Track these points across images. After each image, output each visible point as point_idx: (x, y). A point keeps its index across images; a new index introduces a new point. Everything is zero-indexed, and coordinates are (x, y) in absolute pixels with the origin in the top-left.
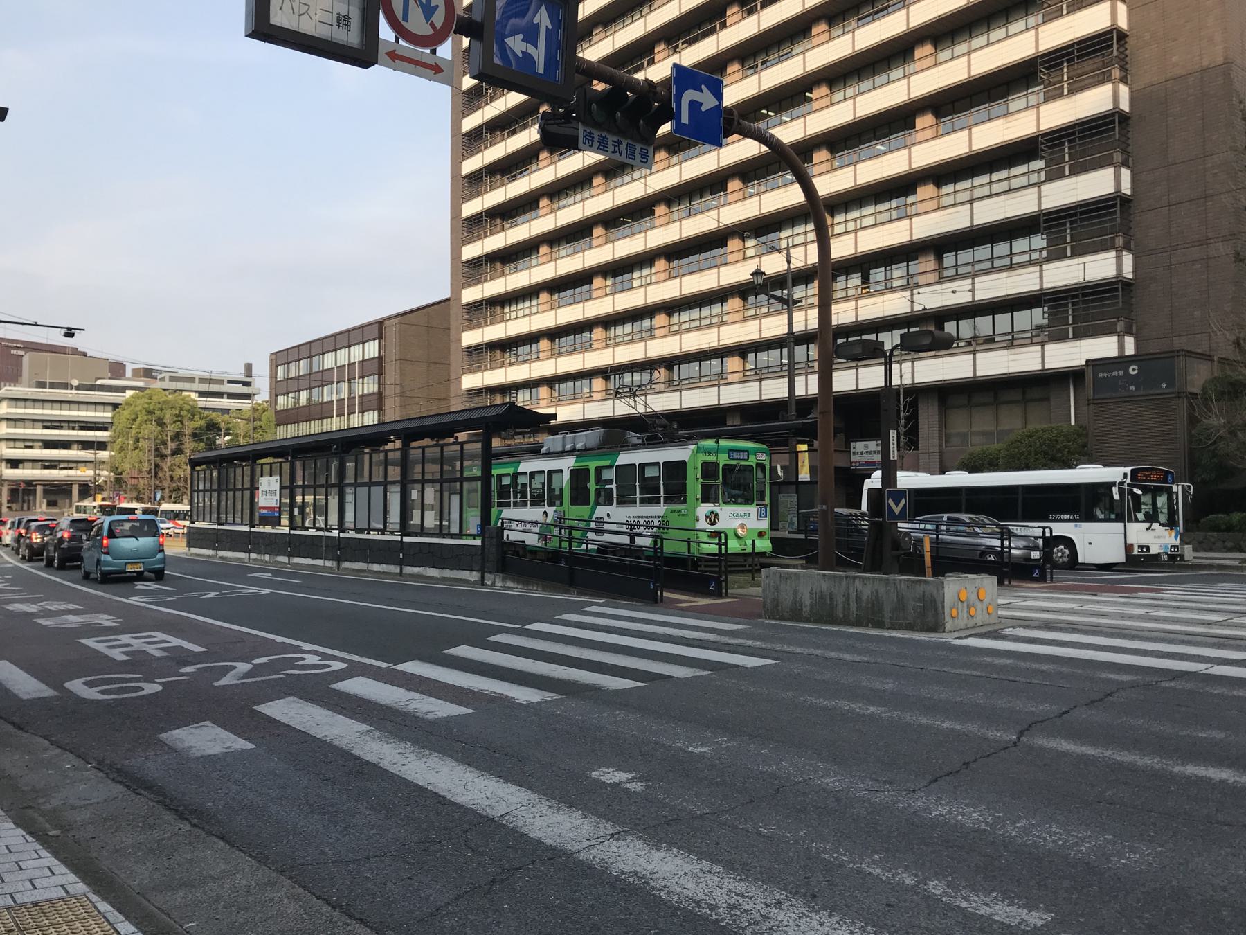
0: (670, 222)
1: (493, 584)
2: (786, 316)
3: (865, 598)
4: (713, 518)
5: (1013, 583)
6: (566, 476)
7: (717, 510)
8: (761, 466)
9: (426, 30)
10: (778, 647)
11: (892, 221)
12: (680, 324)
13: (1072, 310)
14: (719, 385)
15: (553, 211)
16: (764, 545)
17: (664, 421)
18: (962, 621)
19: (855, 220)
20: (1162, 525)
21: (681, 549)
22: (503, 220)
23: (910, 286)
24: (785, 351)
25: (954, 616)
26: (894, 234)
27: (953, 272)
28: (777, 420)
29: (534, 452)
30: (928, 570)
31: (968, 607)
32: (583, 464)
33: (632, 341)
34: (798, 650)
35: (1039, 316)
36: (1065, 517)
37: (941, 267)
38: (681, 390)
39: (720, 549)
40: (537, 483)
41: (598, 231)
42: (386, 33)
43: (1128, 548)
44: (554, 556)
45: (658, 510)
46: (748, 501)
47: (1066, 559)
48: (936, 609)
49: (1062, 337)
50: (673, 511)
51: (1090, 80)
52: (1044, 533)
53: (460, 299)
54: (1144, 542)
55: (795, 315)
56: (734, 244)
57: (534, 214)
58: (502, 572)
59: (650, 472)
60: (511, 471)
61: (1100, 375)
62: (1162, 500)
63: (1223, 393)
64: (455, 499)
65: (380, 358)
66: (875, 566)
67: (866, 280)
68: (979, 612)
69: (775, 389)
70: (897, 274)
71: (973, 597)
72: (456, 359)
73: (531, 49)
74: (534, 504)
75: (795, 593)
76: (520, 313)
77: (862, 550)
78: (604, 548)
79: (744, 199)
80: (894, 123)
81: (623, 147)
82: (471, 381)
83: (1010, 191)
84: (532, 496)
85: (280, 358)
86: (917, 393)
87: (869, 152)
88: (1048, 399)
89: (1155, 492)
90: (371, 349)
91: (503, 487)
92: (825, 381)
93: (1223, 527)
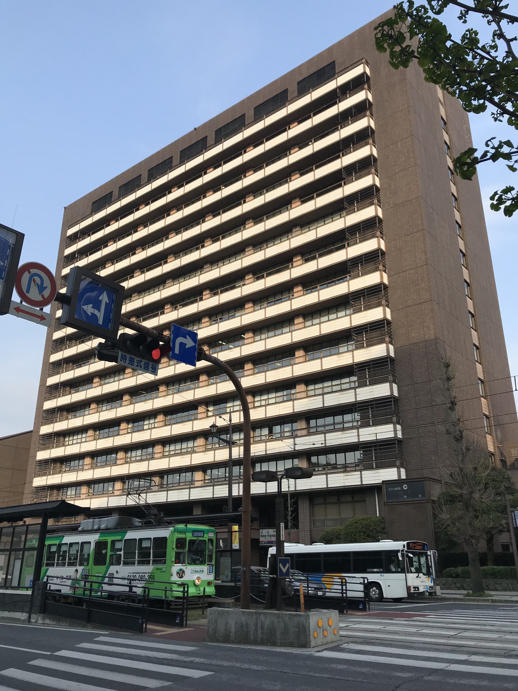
0: (167, 395)
1: (36, 622)
2: (228, 449)
3: (266, 626)
4: (181, 573)
5: (349, 612)
6: (93, 546)
7: (184, 568)
8: (211, 540)
9: (39, 298)
10: (214, 662)
11: (284, 401)
12: (169, 451)
13: (375, 453)
14: (190, 488)
15: (101, 385)
16: (210, 590)
17: (155, 511)
18: (320, 641)
19: (265, 400)
20: (424, 574)
21: (161, 595)
22: (71, 388)
23: (294, 436)
24: (227, 469)
25: (316, 637)
26: (285, 409)
27: (315, 430)
28: (222, 512)
29: (74, 530)
30: (302, 606)
31: (323, 631)
32: (103, 538)
33: (141, 460)
34: (226, 664)
35: (358, 454)
36: (375, 570)
37: (308, 427)
38: (167, 491)
39: (184, 594)
40: (73, 551)
41: (126, 397)
42: (16, 297)
43: (408, 588)
44: (79, 601)
45: (148, 569)
46: (202, 563)
47: (377, 596)
48: (306, 633)
49: (369, 468)
50: (158, 569)
51: (376, 341)
52: (364, 581)
53: (39, 432)
54: (416, 585)
55: (233, 449)
56: (201, 409)
57: (89, 386)
58: (43, 613)
59: (145, 544)
60: (57, 542)
61: (389, 489)
62: (423, 560)
63: (447, 501)
64: (18, 563)
66: (272, 605)
67: (271, 432)
68: (329, 632)
69: (221, 491)
70: (286, 429)
71: (326, 625)
72: (31, 467)
73: (96, 312)
74: (71, 564)
75: (227, 623)
76: (75, 442)
77: (265, 593)
78: (111, 595)
79: (208, 385)
80: (285, 353)
81: (142, 364)
82: (38, 482)
83: (341, 390)
84: (70, 559)
86: (297, 495)
87: (273, 366)
88: (365, 501)
89: (419, 555)
91: (51, 553)
92: (247, 488)
93: (454, 575)
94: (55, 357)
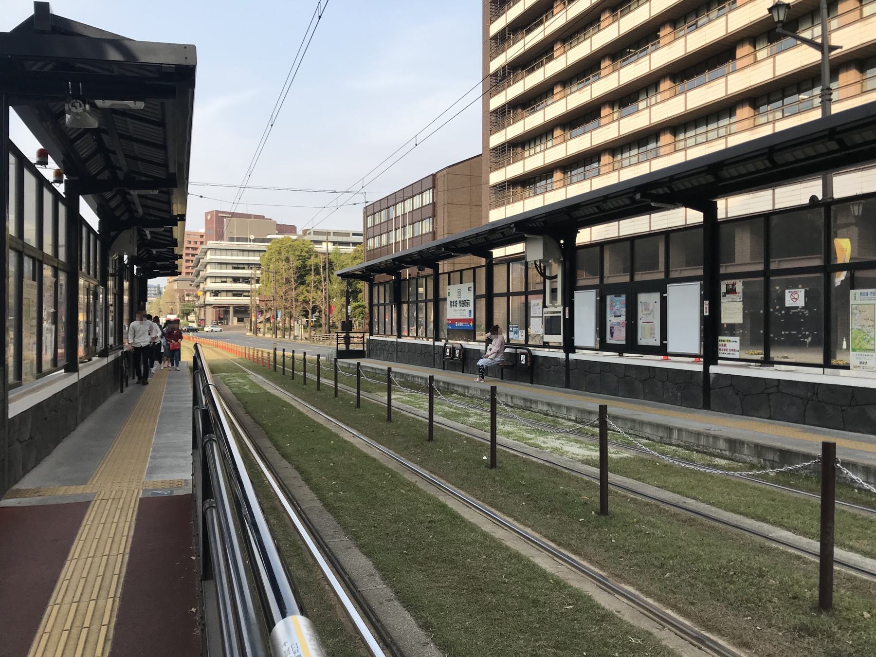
0: (675, 40)
65: (434, 204)
72: (487, 197)
85: (370, 211)
90: (427, 197)
94: (497, 101)
